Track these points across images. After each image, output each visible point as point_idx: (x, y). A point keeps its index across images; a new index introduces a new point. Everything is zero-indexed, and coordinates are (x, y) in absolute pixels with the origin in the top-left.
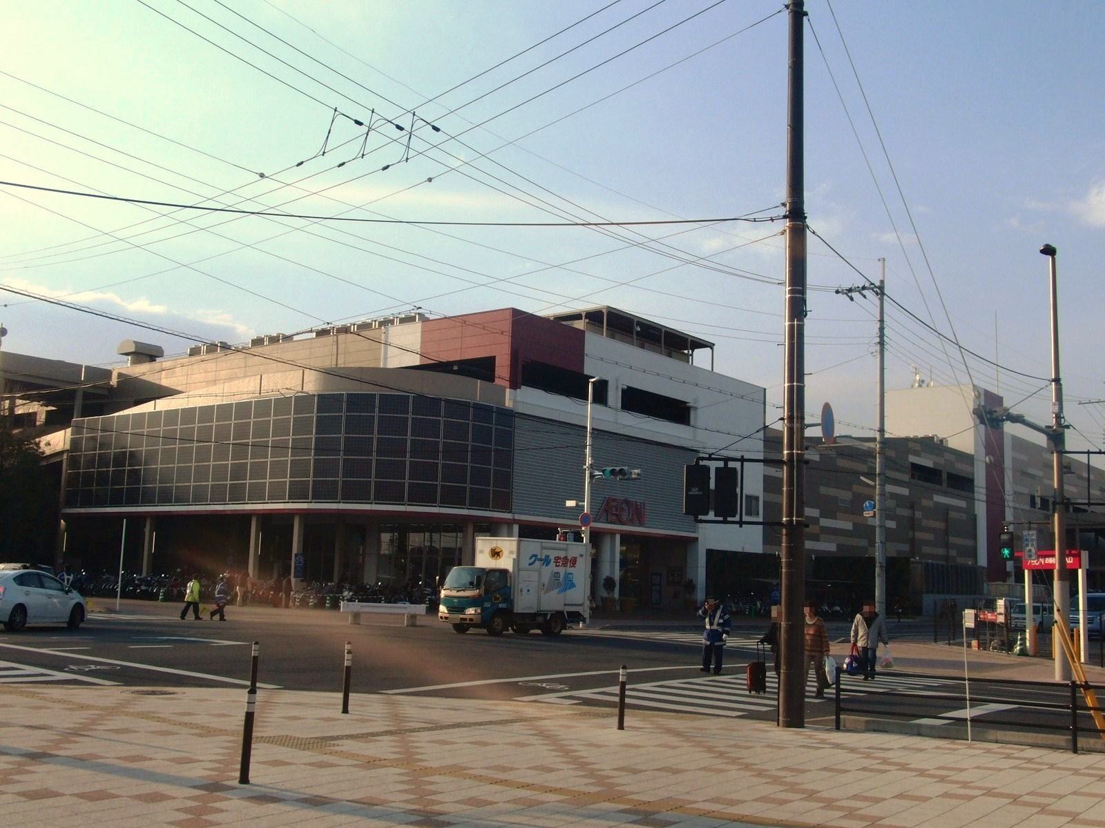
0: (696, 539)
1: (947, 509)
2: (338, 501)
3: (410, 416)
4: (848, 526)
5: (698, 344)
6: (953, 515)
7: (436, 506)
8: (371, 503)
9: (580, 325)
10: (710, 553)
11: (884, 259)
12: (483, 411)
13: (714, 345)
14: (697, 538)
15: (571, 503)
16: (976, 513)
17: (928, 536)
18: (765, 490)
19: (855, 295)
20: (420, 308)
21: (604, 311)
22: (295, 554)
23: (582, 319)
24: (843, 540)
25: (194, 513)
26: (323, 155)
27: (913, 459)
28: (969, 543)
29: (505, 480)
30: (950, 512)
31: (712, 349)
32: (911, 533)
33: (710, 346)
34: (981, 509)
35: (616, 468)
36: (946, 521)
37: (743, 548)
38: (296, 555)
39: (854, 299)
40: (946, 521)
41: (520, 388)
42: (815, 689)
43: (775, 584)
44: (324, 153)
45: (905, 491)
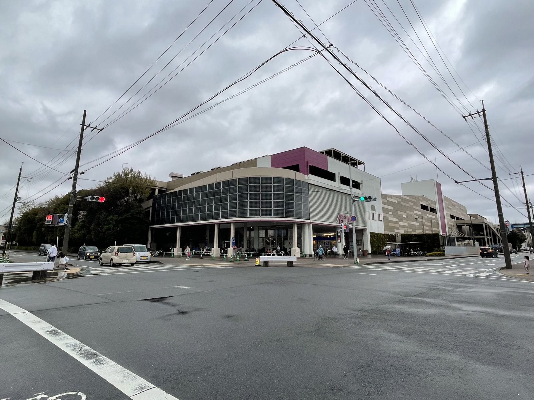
4: (406, 224)
5: (360, 163)
11: (482, 101)
15: (354, 183)
17: (427, 228)
21: (332, 150)
24: (406, 229)
30: (432, 220)
31: (364, 164)
34: (439, 219)
38: (232, 238)
40: (431, 222)
42: (4, 276)
45: (420, 213)
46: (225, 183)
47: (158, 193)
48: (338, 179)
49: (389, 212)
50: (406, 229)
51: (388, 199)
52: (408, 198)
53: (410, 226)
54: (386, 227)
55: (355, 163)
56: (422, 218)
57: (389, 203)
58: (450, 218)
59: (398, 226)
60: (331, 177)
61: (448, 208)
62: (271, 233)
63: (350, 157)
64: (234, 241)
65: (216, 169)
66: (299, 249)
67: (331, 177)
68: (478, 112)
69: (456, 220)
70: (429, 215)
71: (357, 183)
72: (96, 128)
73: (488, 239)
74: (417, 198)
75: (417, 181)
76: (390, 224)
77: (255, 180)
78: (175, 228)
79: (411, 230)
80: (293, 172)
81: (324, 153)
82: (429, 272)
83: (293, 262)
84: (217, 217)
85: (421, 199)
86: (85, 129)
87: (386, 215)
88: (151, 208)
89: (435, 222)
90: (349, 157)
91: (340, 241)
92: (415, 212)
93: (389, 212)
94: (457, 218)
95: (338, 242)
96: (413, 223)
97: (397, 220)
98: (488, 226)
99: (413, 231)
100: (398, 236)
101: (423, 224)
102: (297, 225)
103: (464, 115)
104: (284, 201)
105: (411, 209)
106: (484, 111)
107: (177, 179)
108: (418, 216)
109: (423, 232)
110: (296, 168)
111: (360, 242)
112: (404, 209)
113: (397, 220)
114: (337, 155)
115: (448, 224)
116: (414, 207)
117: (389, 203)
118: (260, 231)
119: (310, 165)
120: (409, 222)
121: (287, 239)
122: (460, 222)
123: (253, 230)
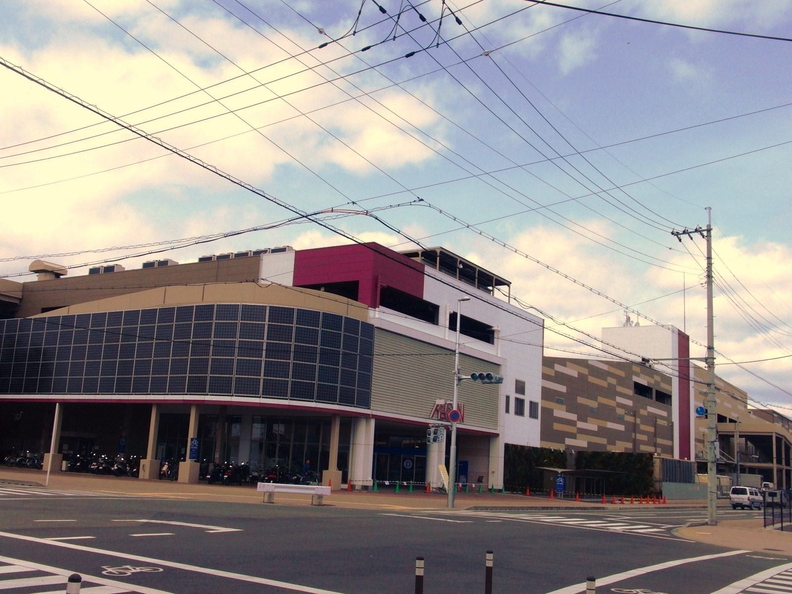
0: (497, 435)
1: (656, 417)
2: (231, 394)
3: (294, 325)
4: (594, 428)
5: (501, 282)
6: (660, 422)
7: (313, 402)
8: (260, 397)
9: (419, 259)
10: (507, 446)
11: (710, 208)
12: (352, 324)
13: (511, 283)
14: (499, 434)
16: (673, 421)
17: (644, 438)
18: (542, 398)
19: (685, 237)
20: (422, 200)
22: (192, 439)
23: (418, 256)
25: (88, 402)
26: (354, 35)
27: (635, 379)
28: (668, 443)
29: (366, 381)
30: (658, 420)
32: (633, 434)
33: (507, 284)
35: (476, 373)
36: (655, 425)
37: (528, 443)
38: (192, 440)
39: (682, 241)
40: (655, 425)
41: (378, 307)
43: (560, 472)
44: (355, 32)
45: (630, 403)
46: (185, 312)
48: (444, 318)
51: (558, 368)
52: (605, 367)
54: (547, 433)
56: (634, 416)
60: (429, 313)
62: (279, 429)
63: (477, 269)
64: (195, 446)
67: (429, 313)
71: (490, 329)
73: (780, 471)
75: (637, 324)
76: (557, 426)
78: (51, 404)
79: (603, 441)
81: (420, 256)
82: (562, 524)
84: (159, 388)
87: (549, 405)
89: (666, 425)
90: (476, 269)
92: (619, 399)
94: (721, 419)
96: (610, 425)
98: (784, 440)
99: (609, 443)
100: (571, 454)
101: (634, 428)
105: (611, 392)
106: (709, 230)
107: (49, 277)
108: (626, 410)
109: (634, 446)
110: (349, 290)
112: (593, 392)
113: (573, 417)
116: (619, 389)
117: (559, 378)
118: (255, 425)
119: (382, 286)
120: (603, 423)
122: (726, 427)
123: (240, 422)
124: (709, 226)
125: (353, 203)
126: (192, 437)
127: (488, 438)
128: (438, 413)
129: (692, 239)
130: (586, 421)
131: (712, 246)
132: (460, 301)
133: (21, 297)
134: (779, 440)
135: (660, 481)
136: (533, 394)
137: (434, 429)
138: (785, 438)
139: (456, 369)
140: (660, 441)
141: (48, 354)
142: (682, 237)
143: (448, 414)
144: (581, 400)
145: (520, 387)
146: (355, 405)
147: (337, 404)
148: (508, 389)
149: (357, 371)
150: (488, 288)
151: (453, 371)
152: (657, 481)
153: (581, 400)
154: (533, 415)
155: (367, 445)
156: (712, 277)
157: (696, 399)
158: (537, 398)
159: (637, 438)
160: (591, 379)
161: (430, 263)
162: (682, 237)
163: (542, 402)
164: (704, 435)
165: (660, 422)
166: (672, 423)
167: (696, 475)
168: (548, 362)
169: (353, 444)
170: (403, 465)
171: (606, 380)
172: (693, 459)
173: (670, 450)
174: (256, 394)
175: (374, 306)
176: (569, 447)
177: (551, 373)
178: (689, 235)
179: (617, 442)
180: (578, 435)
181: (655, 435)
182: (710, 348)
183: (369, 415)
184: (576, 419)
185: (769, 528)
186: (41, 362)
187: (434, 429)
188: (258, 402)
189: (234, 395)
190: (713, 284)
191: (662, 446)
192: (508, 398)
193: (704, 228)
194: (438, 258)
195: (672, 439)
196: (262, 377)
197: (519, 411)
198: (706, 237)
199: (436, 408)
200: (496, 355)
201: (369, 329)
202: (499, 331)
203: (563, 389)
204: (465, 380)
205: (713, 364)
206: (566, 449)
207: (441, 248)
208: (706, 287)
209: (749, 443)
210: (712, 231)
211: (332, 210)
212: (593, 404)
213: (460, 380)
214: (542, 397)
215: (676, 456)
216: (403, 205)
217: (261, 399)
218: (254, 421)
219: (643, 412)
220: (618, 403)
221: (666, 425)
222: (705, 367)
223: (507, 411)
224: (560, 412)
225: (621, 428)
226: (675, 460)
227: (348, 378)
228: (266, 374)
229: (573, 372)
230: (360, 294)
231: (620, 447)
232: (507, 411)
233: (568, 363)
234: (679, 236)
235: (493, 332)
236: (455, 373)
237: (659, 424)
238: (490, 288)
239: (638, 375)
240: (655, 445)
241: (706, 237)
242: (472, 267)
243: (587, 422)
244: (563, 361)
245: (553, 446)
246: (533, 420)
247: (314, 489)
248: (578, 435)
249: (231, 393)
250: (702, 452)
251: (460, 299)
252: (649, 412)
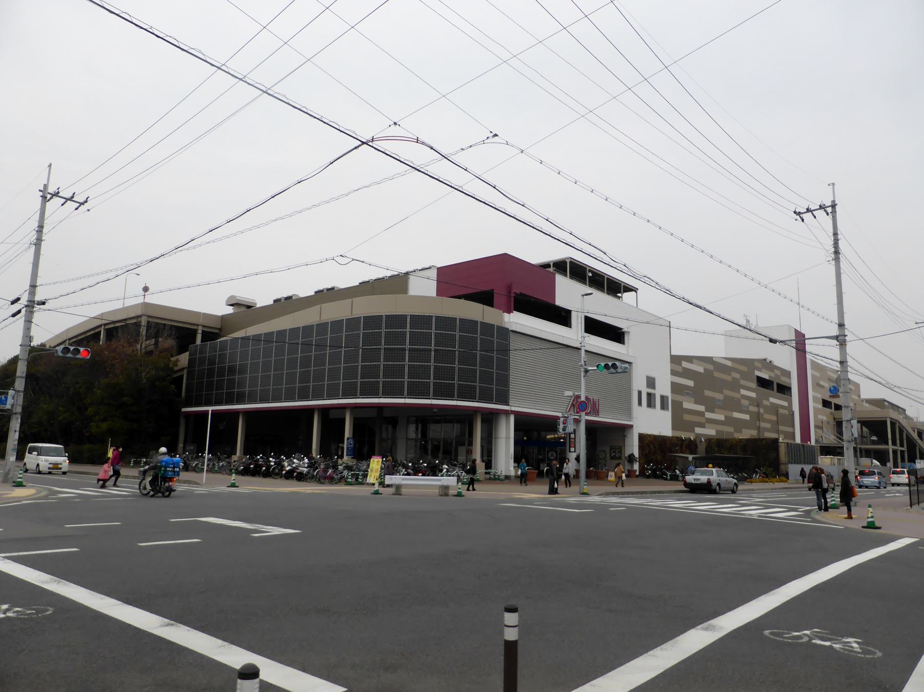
0: (631, 426)
4: (721, 417)
5: (628, 289)
7: (454, 400)
8: (405, 398)
10: (642, 437)
11: (833, 184)
12: (488, 328)
13: (637, 289)
16: (793, 410)
17: (768, 426)
20: (496, 135)
21: (568, 261)
24: (721, 428)
27: (758, 373)
28: (789, 429)
29: (504, 381)
30: (779, 409)
31: (636, 292)
32: (758, 422)
36: (777, 414)
37: (660, 432)
38: (348, 439)
40: (777, 414)
45: (753, 395)
47: (202, 341)
48: (577, 321)
49: (741, 390)
50: (721, 428)
51: (685, 364)
52: (729, 363)
53: (729, 421)
55: (614, 288)
56: (758, 406)
57: (687, 374)
58: (820, 406)
59: (702, 420)
60: (562, 317)
61: (818, 385)
63: (606, 277)
64: (351, 444)
65: (325, 291)
66: (484, 463)
67: (562, 317)
68: (821, 207)
69: (835, 410)
70: (775, 400)
71: (619, 331)
72: (73, 199)
73: (895, 452)
74: (749, 363)
76: (687, 417)
77: (396, 321)
78: (236, 413)
79: (731, 429)
80: (479, 306)
81: (552, 266)
83: (450, 488)
85: (759, 365)
86: (49, 200)
87: (679, 398)
88: (185, 371)
89: (787, 413)
90: (604, 277)
91: (573, 448)
92: (743, 392)
93: (741, 390)
95: (570, 451)
96: (736, 415)
97: (701, 408)
99: (735, 431)
100: (701, 441)
102: (515, 415)
103: (798, 211)
104: (456, 366)
106: (834, 206)
107: (243, 309)
109: (759, 433)
110: (485, 298)
111: (618, 452)
112: (719, 385)
113: (701, 408)
114: (577, 272)
115: (815, 417)
116: (743, 382)
117: (687, 374)
120: (728, 413)
121: (463, 444)
124: (834, 201)
125: (395, 124)
126: (348, 437)
127: (623, 430)
128: (574, 407)
129: (815, 217)
130: (713, 412)
131: (838, 227)
132: (583, 296)
133: (220, 327)
134: (893, 424)
135: (786, 464)
136: (663, 388)
137: (563, 419)
138: (899, 422)
139: (582, 361)
140: (782, 428)
141: (243, 370)
142: (804, 216)
143: (579, 405)
144: (708, 393)
145: (651, 382)
146: (494, 402)
147: (477, 402)
148: (639, 383)
149: (494, 371)
150: (618, 295)
151: (580, 364)
152: (783, 464)
153: (708, 393)
154: (664, 407)
155: (508, 438)
156: (840, 253)
157: (813, 390)
158: (667, 392)
159: (761, 426)
160: (716, 374)
161: (561, 273)
162: (804, 216)
163: (672, 396)
164: (822, 422)
165: (781, 411)
166: (793, 412)
167: (819, 457)
168: (676, 360)
169: (495, 438)
170: (548, 456)
171: (730, 375)
172: (813, 442)
173: (793, 436)
174: (401, 395)
175: (509, 312)
176: (698, 436)
177: (679, 369)
178: (812, 213)
179: (743, 430)
180: (707, 425)
181: (777, 423)
182: (841, 325)
183: (509, 410)
184: (706, 413)
185: (915, 507)
186: (226, 378)
187: (563, 419)
188: (404, 402)
189: (382, 396)
190: (840, 257)
191: (784, 433)
192: (640, 393)
193: (828, 203)
194: (872, 656)
195: (793, 426)
196: (406, 379)
197: (651, 404)
198: (831, 213)
199: (573, 402)
200: (626, 353)
201: (505, 333)
202: (629, 332)
203: (691, 383)
204: (591, 371)
205: (845, 341)
206: (696, 437)
207: (571, 258)
208: (834, 264)
209: (863, 427)
210: (837, 206)
211: (372, 139)
212: (719, 396)
213: (586, 371)
214: (671, 391)
215: (798, 440)
216: (476, 145)
217: (406, 399)
218: (408, 423)
219: (765, 402)
220: (743, 395)
221: (787, 413)
222: (837, 345)
223: (640, 403)
224: (689, 405)
225: (747, 417)
226: (796, 444)
227: (486, 378)
228: (410, 377)
229: (700, 369)
230: (496, 299)
231: (747, 434)
232: (640, 403)
233: (694, 360)
234: (801, 215)
235: (623, 333)
236: (581, 365)
237: (840, 358)
238: (619, 295)
239: (760, 370)
240: (778, 432)
241: (831, 213)
242: (602, 275)
243: (714, 413)
244: (689, 359)
245: (684, 435)
246: (663, 412)
247: (440, 480)
248: (707, 425)
249: (379, 395)
250: (822, 437)
251: (583, 293)
252: (771, 403)
